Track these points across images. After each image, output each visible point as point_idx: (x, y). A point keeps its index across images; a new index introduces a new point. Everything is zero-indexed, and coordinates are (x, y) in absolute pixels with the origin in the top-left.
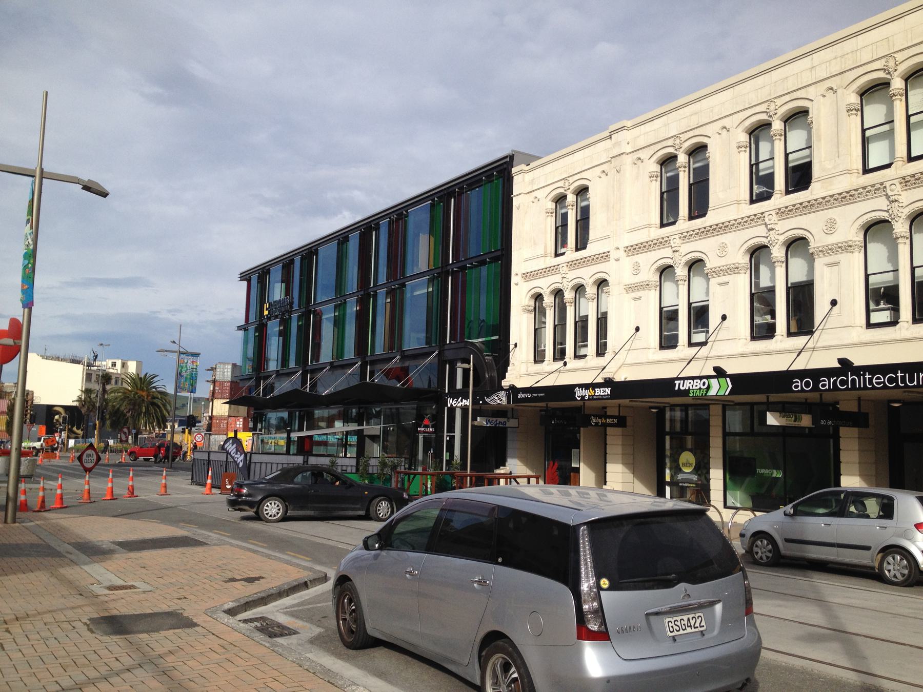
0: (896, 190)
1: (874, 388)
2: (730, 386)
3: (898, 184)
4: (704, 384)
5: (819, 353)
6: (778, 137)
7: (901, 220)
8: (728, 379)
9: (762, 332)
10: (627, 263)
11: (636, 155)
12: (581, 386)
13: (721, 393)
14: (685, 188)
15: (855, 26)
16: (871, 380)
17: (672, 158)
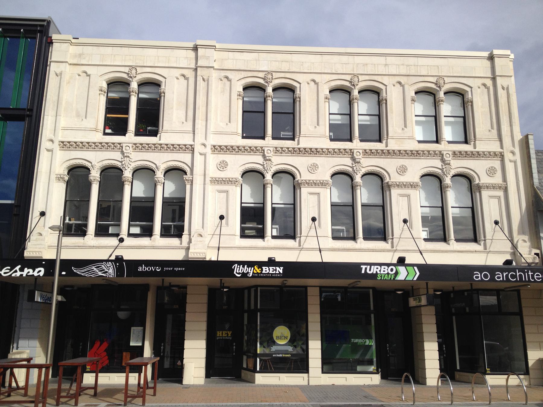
0: (128, 150)
1: (535, 281)
2: (418, 274)
3: (131, 147)
4: (392, 270)
5: (287, 252)
6: (134, 94)
7: (129, 170)
8: (416, 268)
9: (74, 228)
10: (213, 160)
11: (224, 73)
12: (240, 263)
13: (410, 278)
14: (269, 112)
15: (412, 50)
16: (533, 276)
17: (124, 84)
